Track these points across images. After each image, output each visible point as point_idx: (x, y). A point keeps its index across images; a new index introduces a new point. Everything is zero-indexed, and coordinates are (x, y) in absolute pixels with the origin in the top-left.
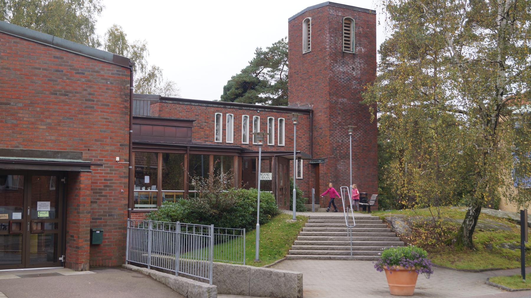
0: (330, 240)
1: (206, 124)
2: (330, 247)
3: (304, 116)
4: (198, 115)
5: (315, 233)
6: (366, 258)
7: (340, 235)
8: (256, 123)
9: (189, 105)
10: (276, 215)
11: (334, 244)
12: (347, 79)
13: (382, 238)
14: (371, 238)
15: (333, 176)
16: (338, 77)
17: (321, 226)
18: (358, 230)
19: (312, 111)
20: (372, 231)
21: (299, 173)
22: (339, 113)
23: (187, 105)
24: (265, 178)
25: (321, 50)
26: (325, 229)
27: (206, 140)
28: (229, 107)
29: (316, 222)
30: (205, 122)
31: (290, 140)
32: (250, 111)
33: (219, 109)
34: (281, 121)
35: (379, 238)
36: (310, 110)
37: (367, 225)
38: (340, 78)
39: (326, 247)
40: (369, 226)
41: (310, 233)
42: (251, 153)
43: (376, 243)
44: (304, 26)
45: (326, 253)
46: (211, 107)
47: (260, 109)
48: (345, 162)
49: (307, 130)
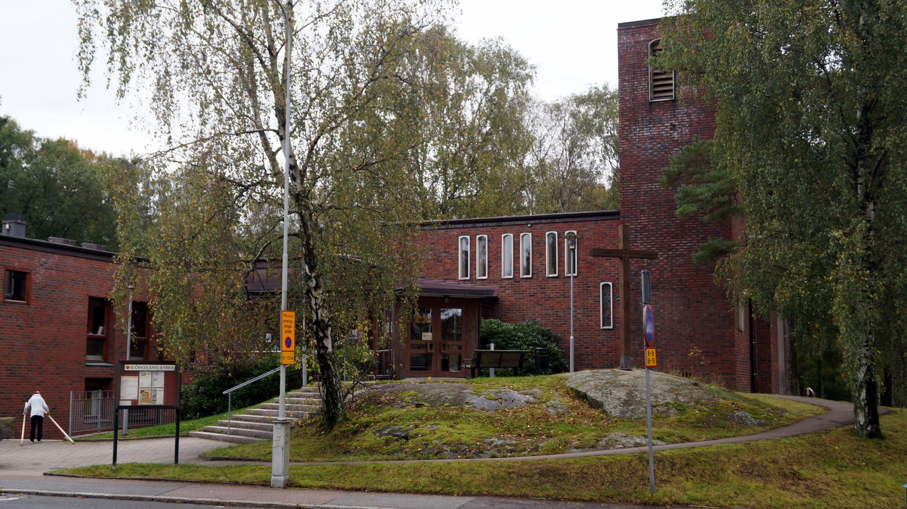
1: (445, 254)
4: (434, 244)
8: (494, 245)
12: (659, 148)
16: (638, 147)
22: (643, 211)
27: (447, 277)
28: (481, 225)
30: (445, 252)
31: (589, 265)
32: (516, 227)
33: (466, 230)
38: (644, 149)
47: (533, 222)
48: (655, 295)
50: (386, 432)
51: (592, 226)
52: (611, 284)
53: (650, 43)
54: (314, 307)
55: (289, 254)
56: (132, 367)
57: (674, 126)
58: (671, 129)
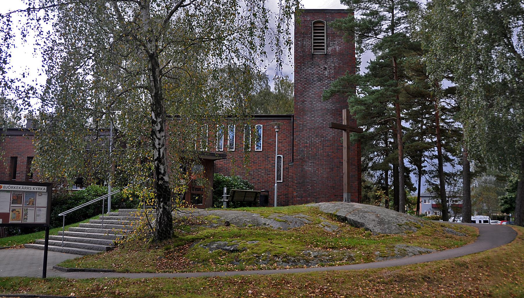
50: (214, 246)
52: (282, 156)
53: (313, 22)
54: (157, 147)
56: (4, 187)
57: (326, 68)
58: (324, 70)
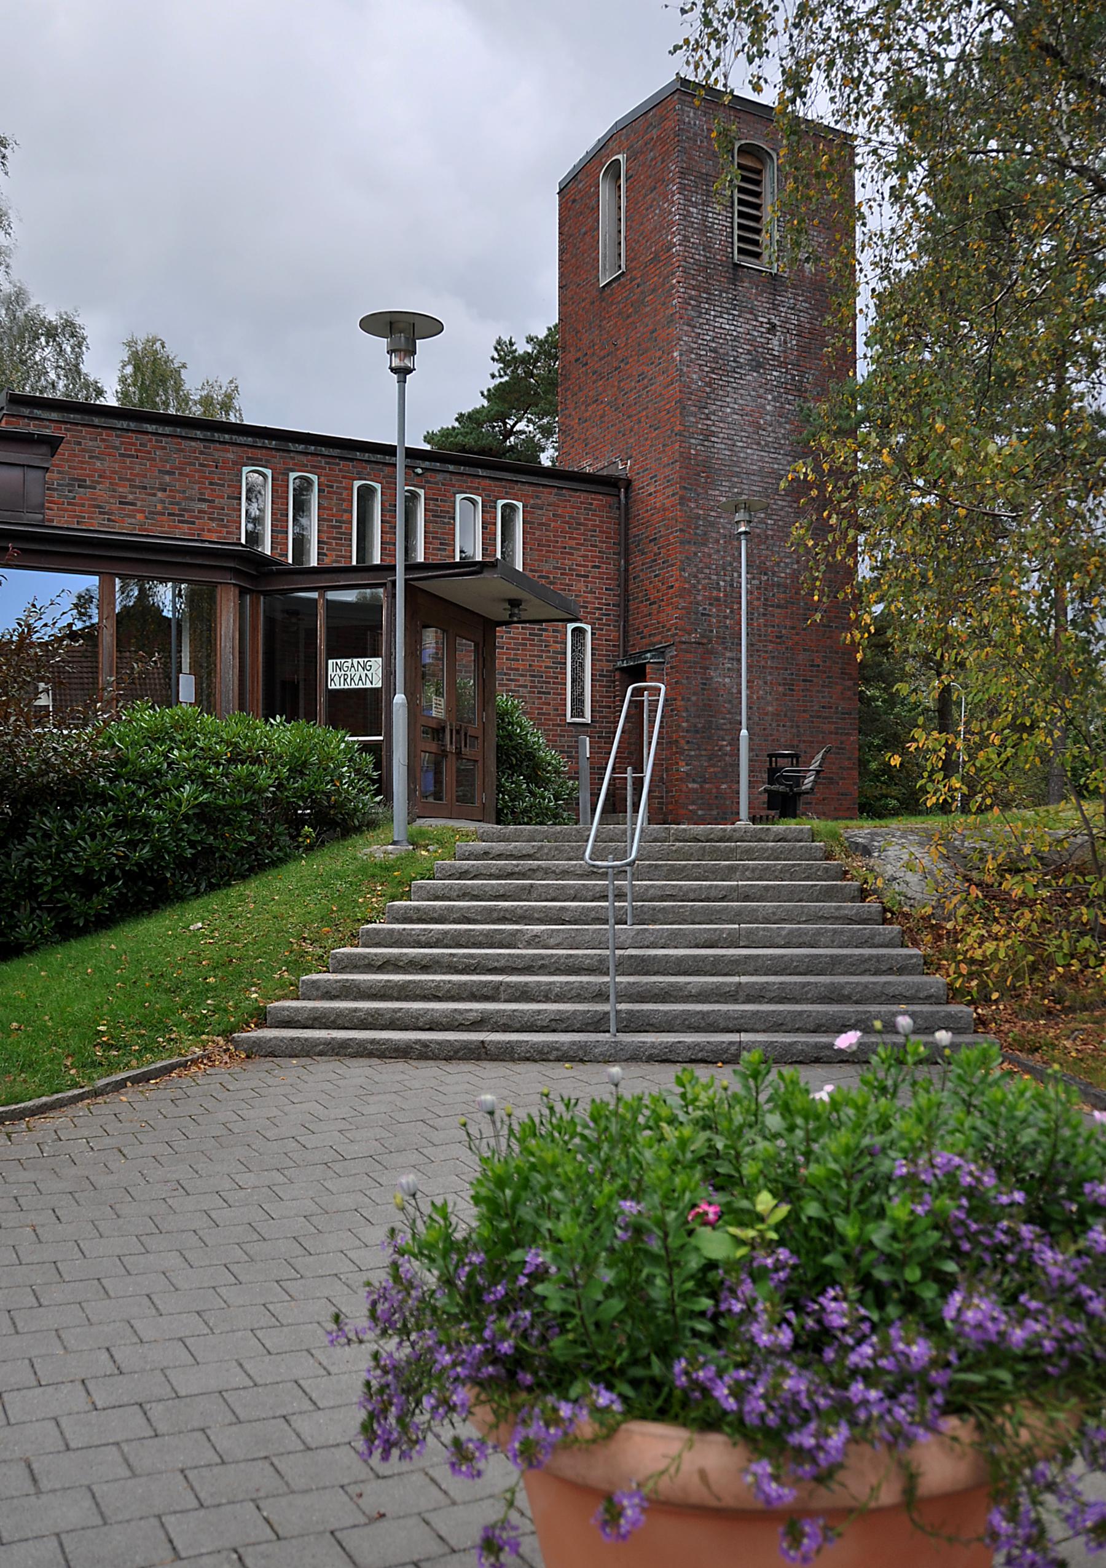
0: (529, 945)
2: (508, 984)
3: (598, 501)
5: (461, 908)
6: (690, 1047)
7: (593, 915)
9: (133, 431)
10: (358, 830)
11: (542, 966)
13: (806, 933)
14: (750, 932)
15: (693, 709)
17: (510, 875)
18: (692, 889)
19: (628, 483)
20: (762, 895)
21: (578, 701)
23: (127, 430)
24: (356, 679)
25: (656, 259)
26: (523, 888)
28: (301, 447)
29: (495, 852)
30: (200, 500)
33: (259, 453)
34: (509, 510)
35: (791, 931)
36: (618, 479)
37: (746, 868)
39: (486, 984)
40: (754, 869)
41: (434, 908)
42: (295, 577)
43: (772, 958)
44: (605, 191)
45: (472, 1016)
46: (224, 443)
47: (427, 464)
49: (608, 548)
51: (553, 499)
52: (588, 628)
55: (884, 956)
